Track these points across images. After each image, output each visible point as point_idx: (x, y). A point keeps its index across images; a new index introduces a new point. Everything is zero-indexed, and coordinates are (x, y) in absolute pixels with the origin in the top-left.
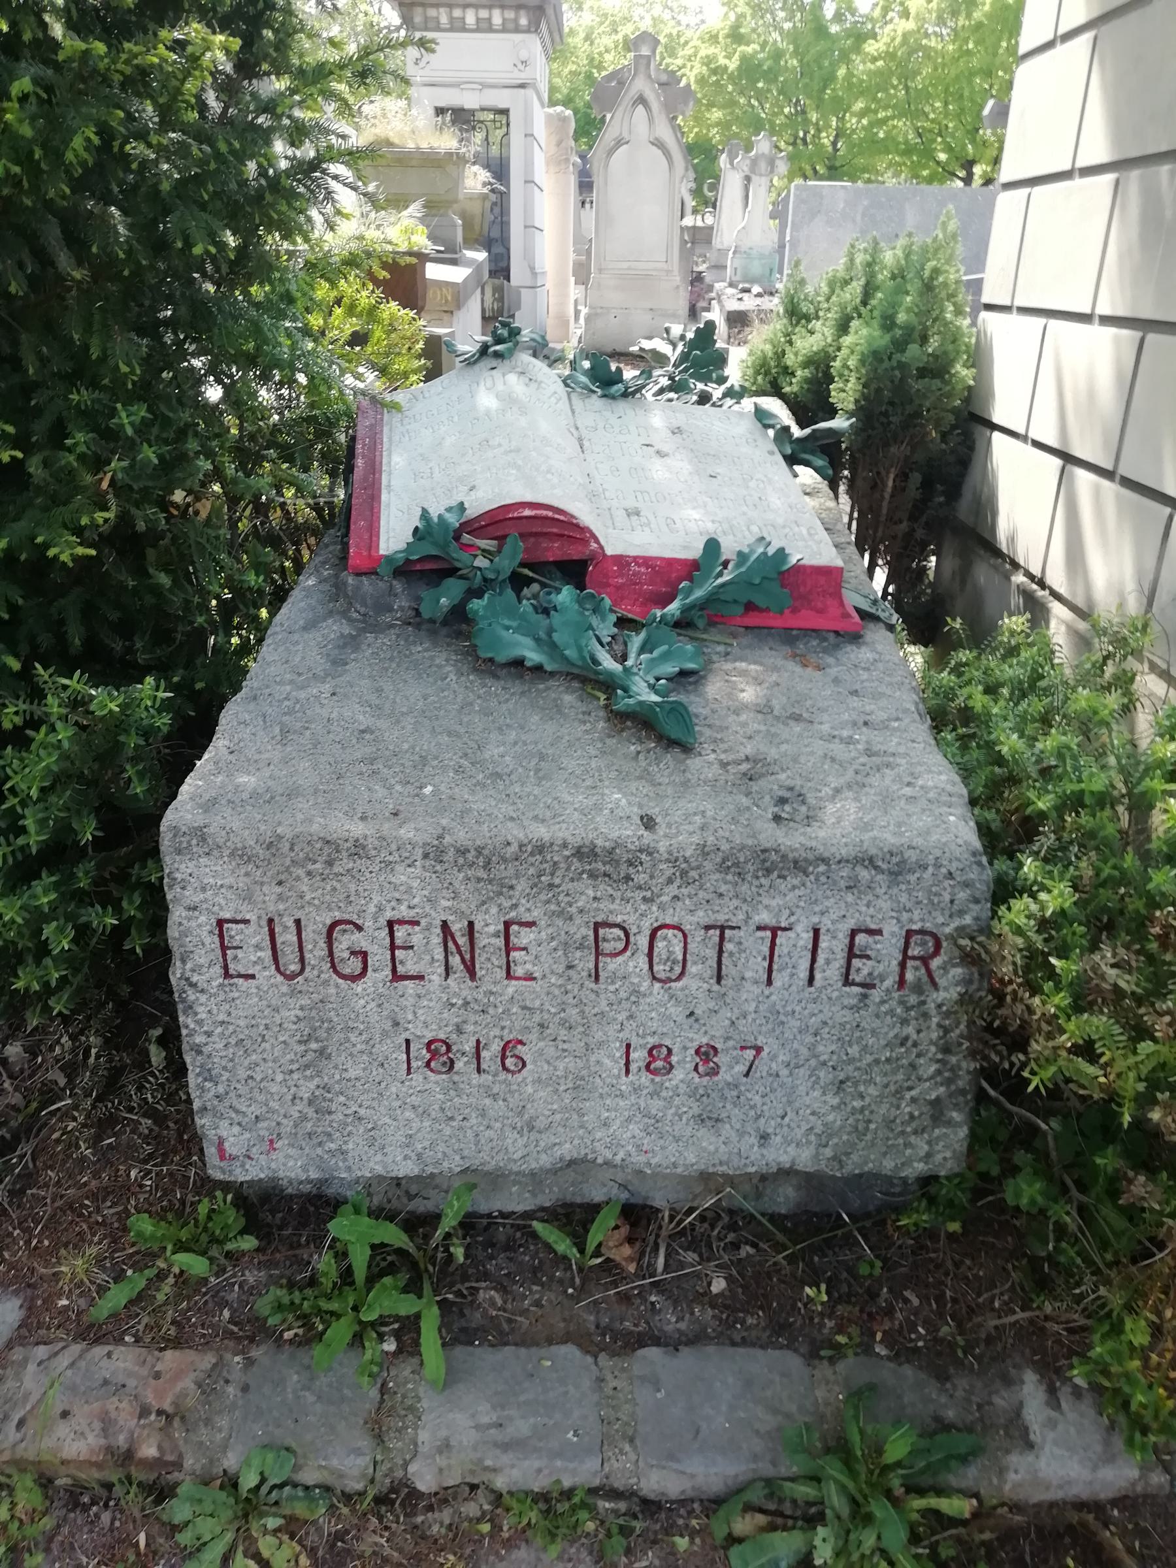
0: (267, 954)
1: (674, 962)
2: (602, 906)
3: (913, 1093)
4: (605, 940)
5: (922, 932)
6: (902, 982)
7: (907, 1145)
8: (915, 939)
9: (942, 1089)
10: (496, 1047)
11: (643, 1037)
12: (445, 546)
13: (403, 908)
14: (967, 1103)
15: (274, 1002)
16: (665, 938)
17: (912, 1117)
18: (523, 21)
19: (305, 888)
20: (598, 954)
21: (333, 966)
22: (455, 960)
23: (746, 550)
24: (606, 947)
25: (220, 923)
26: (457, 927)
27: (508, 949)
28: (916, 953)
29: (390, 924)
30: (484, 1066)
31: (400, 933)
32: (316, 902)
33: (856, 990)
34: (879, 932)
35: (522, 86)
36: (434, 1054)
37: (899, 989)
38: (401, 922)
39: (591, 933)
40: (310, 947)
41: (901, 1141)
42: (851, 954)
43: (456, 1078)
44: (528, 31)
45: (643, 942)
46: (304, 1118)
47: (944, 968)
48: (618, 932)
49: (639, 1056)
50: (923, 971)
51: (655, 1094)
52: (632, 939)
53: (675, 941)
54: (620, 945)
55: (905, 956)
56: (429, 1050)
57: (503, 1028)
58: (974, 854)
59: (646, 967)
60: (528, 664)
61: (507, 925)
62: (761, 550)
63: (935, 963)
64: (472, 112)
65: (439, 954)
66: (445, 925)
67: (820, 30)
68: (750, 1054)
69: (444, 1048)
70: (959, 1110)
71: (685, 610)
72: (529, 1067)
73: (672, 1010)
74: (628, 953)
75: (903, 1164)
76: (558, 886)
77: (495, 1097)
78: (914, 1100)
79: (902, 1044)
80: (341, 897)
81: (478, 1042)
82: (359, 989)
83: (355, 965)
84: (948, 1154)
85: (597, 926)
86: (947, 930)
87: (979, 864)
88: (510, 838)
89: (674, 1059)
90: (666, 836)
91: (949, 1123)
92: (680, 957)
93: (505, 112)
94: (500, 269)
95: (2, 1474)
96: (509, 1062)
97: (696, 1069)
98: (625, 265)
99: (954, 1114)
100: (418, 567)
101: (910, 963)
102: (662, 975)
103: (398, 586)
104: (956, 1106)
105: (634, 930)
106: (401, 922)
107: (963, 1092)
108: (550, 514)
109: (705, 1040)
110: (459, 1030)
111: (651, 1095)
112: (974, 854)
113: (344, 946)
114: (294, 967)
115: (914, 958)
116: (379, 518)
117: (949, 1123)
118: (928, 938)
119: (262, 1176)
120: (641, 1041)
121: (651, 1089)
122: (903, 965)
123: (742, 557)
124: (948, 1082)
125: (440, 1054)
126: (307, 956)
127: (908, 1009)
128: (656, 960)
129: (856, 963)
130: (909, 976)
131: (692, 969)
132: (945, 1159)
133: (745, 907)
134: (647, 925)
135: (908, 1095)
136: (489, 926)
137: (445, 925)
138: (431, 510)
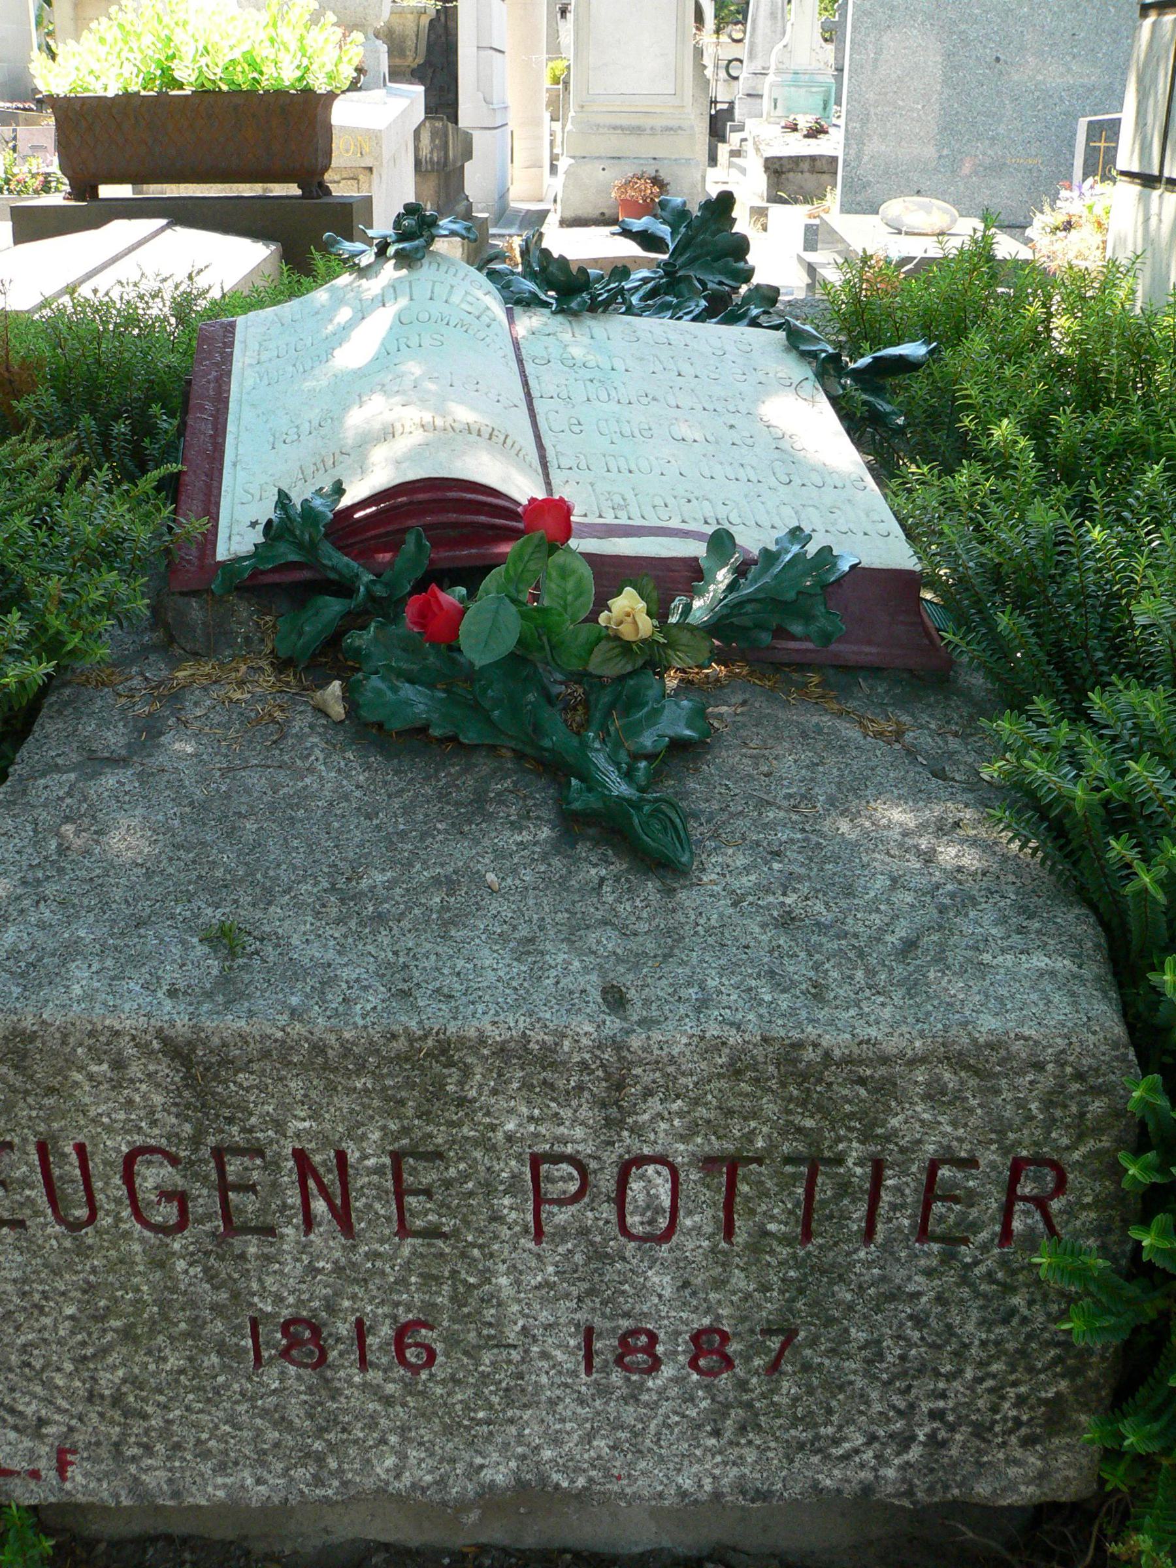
1: (659, 1210)
2: (542, 1130)
3: (1022, 1389)
4: (551, 1180)
5: (1038, 1161)
6: (1006, 1234)
9: (1063, 1385)
10: (386, 1331)
11: (612, 1318)
12: (311, 548)
13: (235, 1130)
14: (1100, 1400)
15: (53, 1259)
16: (642, 1177)
17: (1018, 1423)
19: (87, 1100)
20: (539, 1200)
21: (137, 1213)
22: (319, 1206)
23: (773, 548)
24: (552, 1190)
27: (400, 1193)
28: (1027, 1190)
29: (218, 1154)
30: (370, 1357)
31: (234, 1167)
32: (105, 1120)
33: (935, 1247)
36: (295, 1342)
37: (1001, 1245)
38: (237, 1151)
39: (527, 1170)
40: (100, 1184)
41: (1001, 1456)
43: (329, 1374)
45: (606, 1182)
47: (1070, 1212)
48: (566, 1168)
50: (1038, 1216)
51: (633, 1398)
52: (591, 1178)
53: (659, 1181)
54: (573, 1187)
55: (1012, 1197)
56: (285, 1333)
57: (397, 1304)
58: (1115, 1046)
59: (614, 1218)
60: (436, 732)
61: (397, 1158)
62: (795, 549)
63: (1055, 1205)
65: (293, 1198)
66: (300, 1156)
67: (860, 301)
68: (775, 1343)
69: (307, 1334)
70: (1090, 1411)
72: (440, 1359)
73: (656, 1279)
74: (586, 1200)
75: (1004, 1490)
76: (474, 1100)
77: (388, 1401)
78: (1020, 1401)
79: (1005, 1321)
80: (142, 1113)
81: (359, 1323)
82: (176, 1246)
83: (167, 1213)
84: (1071, 1473)
85: (536, 1161)
86: (1076, 1156)
87: (1124, 1059)
88: (394, 1027)
89: (660, 1349)
90: (642, 1022)
91: (1075, 1428)
92: (667, 1203)
94: (443, 101)
96: (410, 1354)
97: (693, 1364)
99: (1083, 1418)
100: (276, 578)
101: (1019, 1206)
102: (639, 1230)
104: (1085, 1407)
105: (593, 1165)
106: (237, 1151)
107: (1096, 1386)
108: (453, 517)
109: (706, 1321)
110: (331, 1307)
111: (625, 1400)
112: (1115, 1046)
113: (149, 1184)
114: (82, 1213)
115: (1025, 1199)
116: (218, 505)
117: (1075, 1428)
118: (1047, 1170)
119: (52, 1499)
120: (608, 1325)
121: (625, 1391)
122: (1007, 1214)
123: (769, 557)
124: (1071, 1374)
125: (305, 1339)
126: (100, 1197)
128: (629, 1208)
129: (938, 1208)
130: (1017, 1225)
132: (1066, 1479)
133: (872, 110)
134: (610, 1157)
135: (1011, 1392)
136: (369, 1155)
137: (300, 1156)
138: (293, 495)
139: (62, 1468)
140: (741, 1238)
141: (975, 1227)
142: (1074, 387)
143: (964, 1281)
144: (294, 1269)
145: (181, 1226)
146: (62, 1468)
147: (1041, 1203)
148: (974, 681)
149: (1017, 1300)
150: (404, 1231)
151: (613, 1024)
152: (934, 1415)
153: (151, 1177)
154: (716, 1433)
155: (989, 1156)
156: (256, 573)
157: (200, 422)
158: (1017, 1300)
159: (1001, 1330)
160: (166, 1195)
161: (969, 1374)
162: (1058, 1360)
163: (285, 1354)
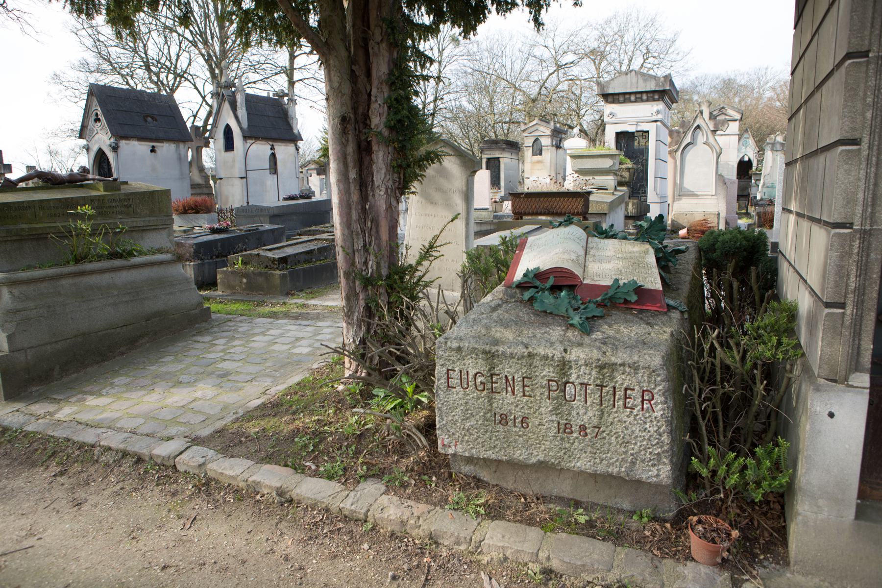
0: (459, 381)
7: (650, 471)
8: (646, 393)
10: (520, 419)
18: (656, 97)
25: (448, 370)
26: (510, 378)
27: (524, 386)
31: (494, 378)
34: (633, 390)
35: (656, 121)
42: (626, 398)
44: (658, 100)
46: (465, 435)
48: (555, 383)
49: (562, 427)
55: (643, 400)
61: (524, 378)
63: (652, 402)
64: (633, 133)
68: (597, 430)
71: (603, 300)
78: (651, 453)
93: (647, 132)
95: (380, 3)
98: (354, 212)
103: (518, 291)
124: (661, 447)
127: (646, 418)
130: (645, 406)
131: (577, 398)
137: (506, 376)
139: (456, 445)
140: (588, 403)
141: (636, 406)
142: (724, 229)
143: (635, 419)
144: (506, 401)
145: (483, 390)
146: (456, 445)
147: (650, 401)
148: (733, 482)
149: (647, 426)
150: (524, 395)
151: (564, 354)
152: (632, 455)
153: (479, 379)
154: (585, 452)
155: (637, 388)
156: (520, 284)
157: (777, 275)
158: (647, 426)
159: (644, 434)
160: (481, 383)
161: (639, 444)
162: (658, 443)
163: (500, 422)
